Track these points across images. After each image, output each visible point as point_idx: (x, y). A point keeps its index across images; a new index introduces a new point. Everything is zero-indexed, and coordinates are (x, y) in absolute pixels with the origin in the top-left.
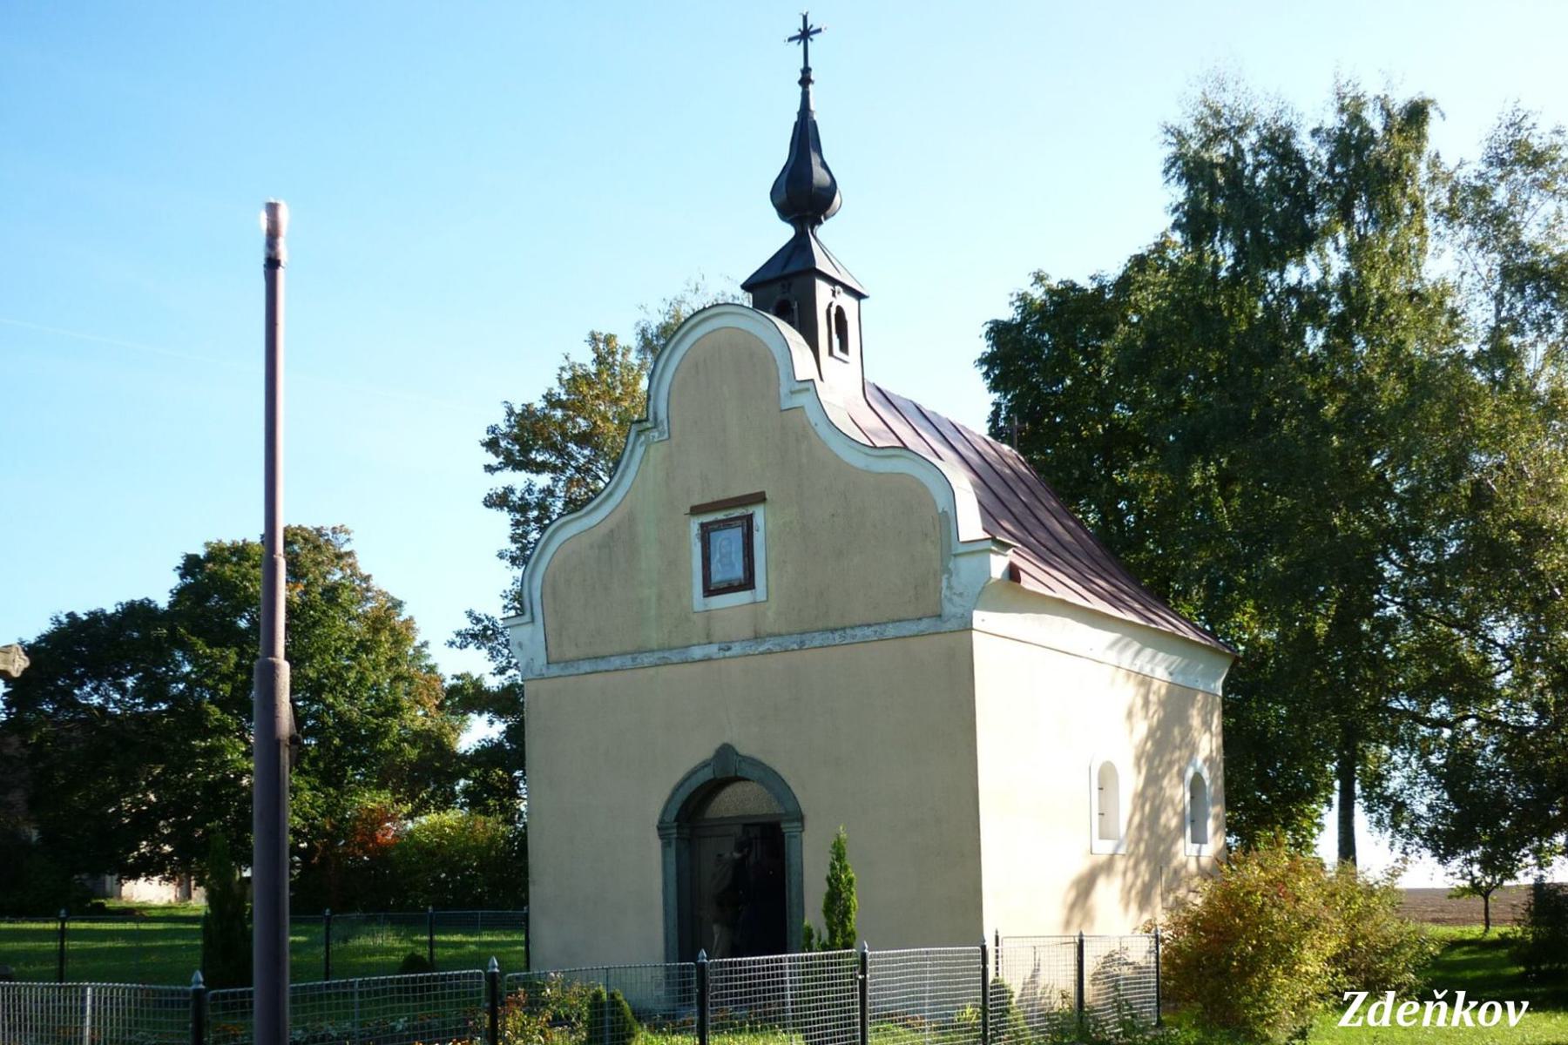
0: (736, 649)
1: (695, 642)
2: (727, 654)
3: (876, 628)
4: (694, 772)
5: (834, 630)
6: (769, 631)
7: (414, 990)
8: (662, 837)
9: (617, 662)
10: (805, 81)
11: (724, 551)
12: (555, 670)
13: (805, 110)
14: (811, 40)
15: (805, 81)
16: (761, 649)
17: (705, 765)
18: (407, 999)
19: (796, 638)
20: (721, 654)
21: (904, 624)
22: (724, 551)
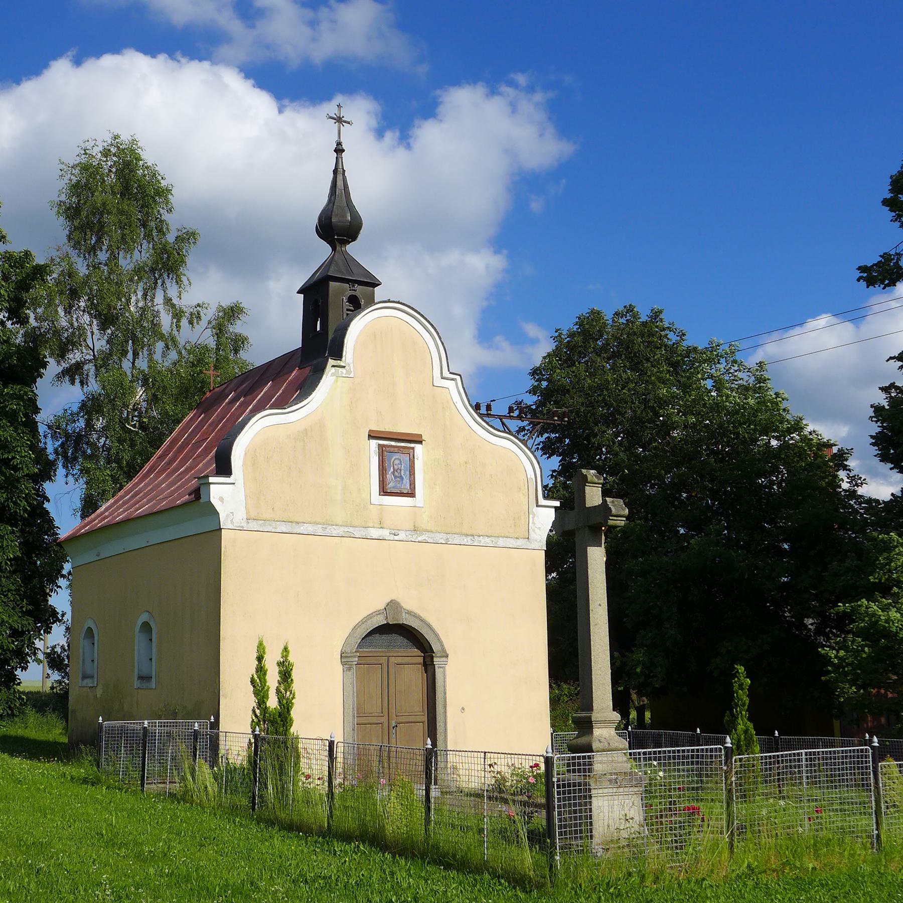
0: (402, 535)
1: (371, 525)
2: (396, 538)
3: (493, 539)
4: (370, 617)
5: (467, 535)
6: (424, 528)
7: (692, 757)
8: (343, 664)
9: (310, 529)
10: (339, 150)
11: (396, 467)
12: (254, 525)
13: (338, 171)
14: (335, 123)
15: (339, 150)
16: (420, 539)
17: (378, 613)
18: (679, 764)
19: (445, 536)
20: (392, 537)
21: (508, 540)
22: (396, 467)
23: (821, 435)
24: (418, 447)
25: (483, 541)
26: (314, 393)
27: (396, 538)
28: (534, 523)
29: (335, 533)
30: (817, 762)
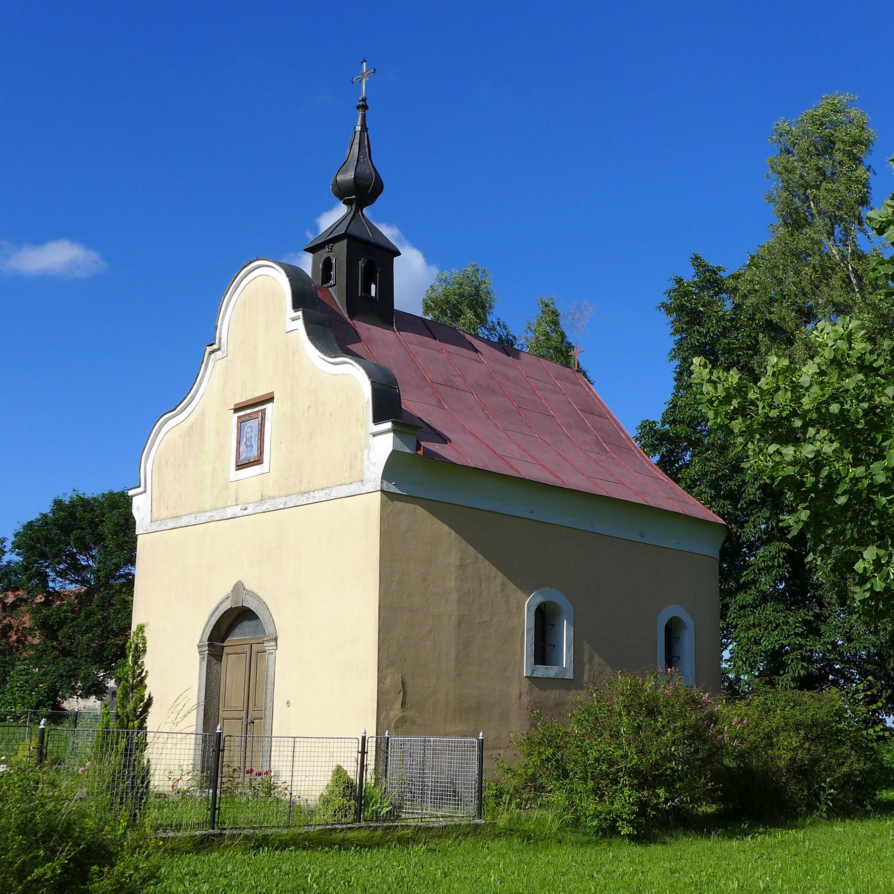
3: (326, 491)
16: (264, 509)
19: (283, 500)
23: (427, 291)
24: (269, 407)
25: (317, 496)
26: (310, 342)
27: (246, 513)
28: (369, 459)
29: (202, 520)
30: (449, 793)
